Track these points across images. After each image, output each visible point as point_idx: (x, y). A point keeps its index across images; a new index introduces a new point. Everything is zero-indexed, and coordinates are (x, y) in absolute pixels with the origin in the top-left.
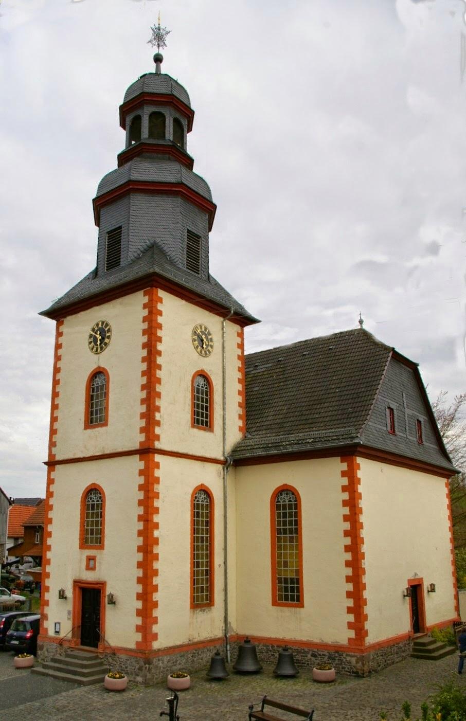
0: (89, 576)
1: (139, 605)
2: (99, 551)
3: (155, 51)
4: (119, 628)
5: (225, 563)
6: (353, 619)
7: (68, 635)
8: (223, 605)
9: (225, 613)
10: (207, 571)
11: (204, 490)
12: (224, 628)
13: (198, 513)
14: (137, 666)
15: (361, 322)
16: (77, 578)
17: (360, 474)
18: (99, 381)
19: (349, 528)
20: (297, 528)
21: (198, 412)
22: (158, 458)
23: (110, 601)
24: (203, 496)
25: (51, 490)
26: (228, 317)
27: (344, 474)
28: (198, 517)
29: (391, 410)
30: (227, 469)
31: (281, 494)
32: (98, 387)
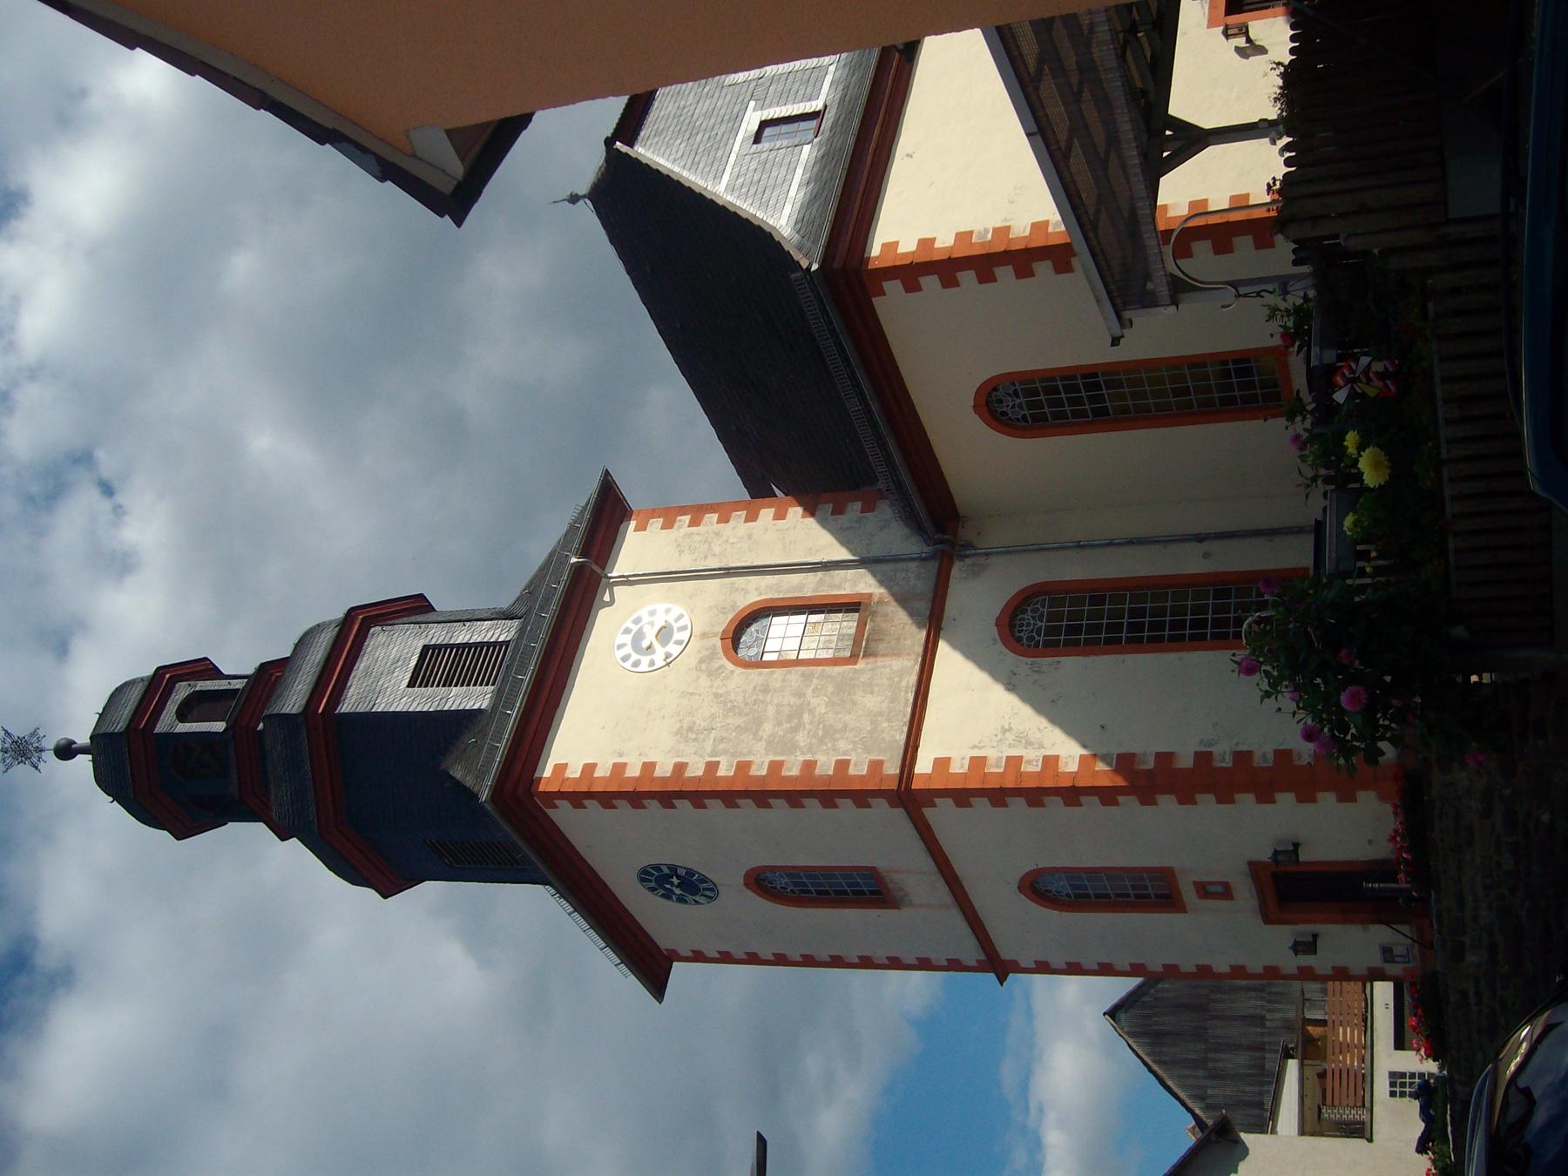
3: (50, 756)
5: (1199, 538)
11: (1013, 617)
15: (574, 199)
17: (908, 246)
19: (1049, 263)
22: (923, 766)
26: (598, 570)
29: (764, 124)
31: (1004, 414)
32: (1030, 405)
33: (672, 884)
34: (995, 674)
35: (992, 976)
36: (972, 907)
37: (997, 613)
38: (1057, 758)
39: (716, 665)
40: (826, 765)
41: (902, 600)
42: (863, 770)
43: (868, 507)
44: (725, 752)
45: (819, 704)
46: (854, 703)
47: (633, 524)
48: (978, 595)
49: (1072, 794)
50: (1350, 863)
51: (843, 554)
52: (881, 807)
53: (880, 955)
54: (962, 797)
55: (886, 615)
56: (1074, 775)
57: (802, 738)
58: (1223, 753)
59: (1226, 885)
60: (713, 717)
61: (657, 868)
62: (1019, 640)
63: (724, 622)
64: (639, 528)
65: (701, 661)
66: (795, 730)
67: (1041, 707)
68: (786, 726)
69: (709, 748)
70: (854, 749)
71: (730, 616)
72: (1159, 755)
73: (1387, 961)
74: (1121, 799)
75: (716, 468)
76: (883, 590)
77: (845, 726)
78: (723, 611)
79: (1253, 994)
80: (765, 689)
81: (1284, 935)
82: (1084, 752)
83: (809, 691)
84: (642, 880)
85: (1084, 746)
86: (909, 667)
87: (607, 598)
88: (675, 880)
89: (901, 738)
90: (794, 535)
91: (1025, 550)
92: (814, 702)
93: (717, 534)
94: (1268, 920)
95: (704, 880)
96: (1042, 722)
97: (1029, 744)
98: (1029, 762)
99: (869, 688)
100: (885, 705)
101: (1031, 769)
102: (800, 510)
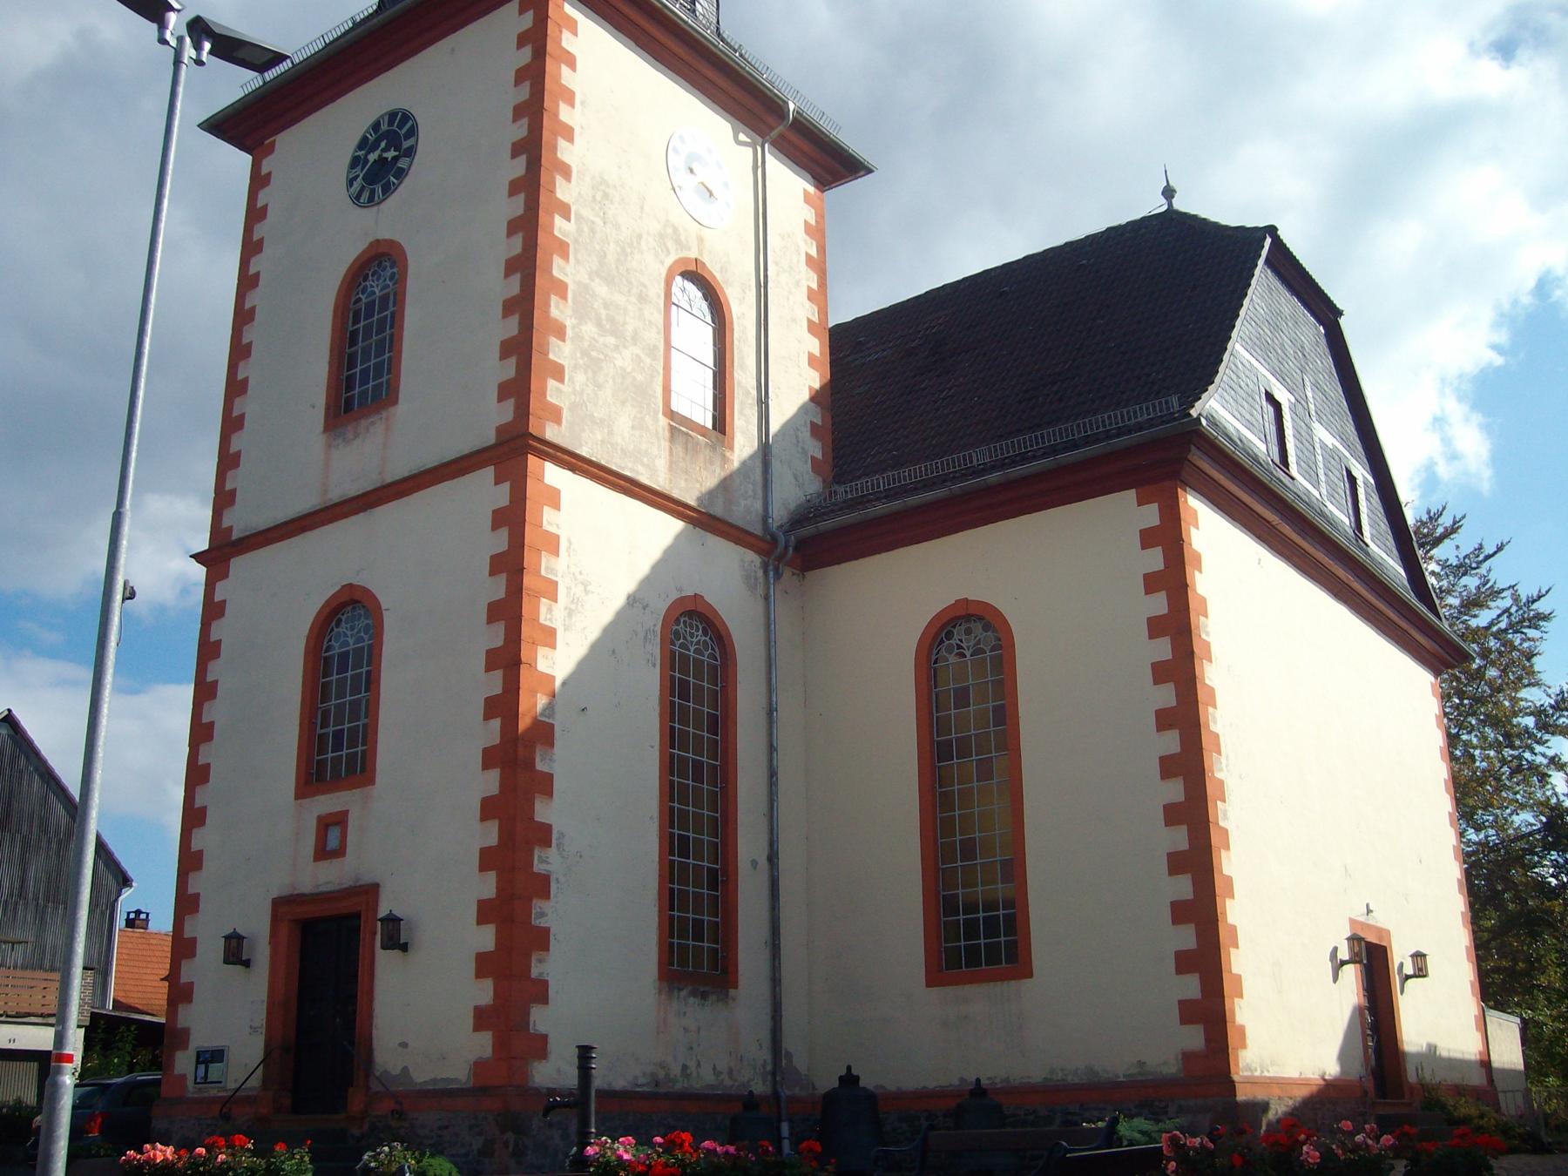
0: (330, 876)
1: (486, 938)
2: (357, 793)
4: (424, 1016)
5: (773, 858)
6: (1194, 939)
7: (249, 1084)
8: (764, 989)
9: (773, 1018)
10: (713, 873)
12: (769, 1068)
13: (684, 840)
14: (477, 1143)
15: (1169, 193)
16: (285, 892)
18: (347, 637)
20: (1015, 942)
21: (683, 815)
22: (554, 475)
23: (391, 938)
24: (700, 636)
25: (199, 802)
26: (774, 134)
27: (1148, 538)
28: (684, 853)
29: (1277, 406)
30: (776, 570)
31: (949, 635)
32: (344, 656)
33: (386, 150)
34: (646, 582)
35: (204, 545)
36: (323, 524)
37: (709, 599)
38: (553, 646)
39: (670, 244)
40: (560, 352)
41: (725, 485)
42: (551, 398)
43: (816, 465)
44: (580, 231)
45: (624, 359)
46: (623, 403)
47: (811, 189)
48: (727, 577)
49: (508, 660)
50: (370, 1017)
51: (774, 427)
52: (505, 413)
53: (247, 406)
54: (512, 519)
55: (711, 463)
56: (532, 666)
57: (589, 329)
58: (547, 861)
59: (340, 852)
60: (617, 227)
61: (413, 132)
62: (677, 621)
63: (715, 268)
64: (806, 193)
65: (675, 229)
66: (599, 324)
67: (610, 631)
68: (603, 313)
69: (585, 212)
70: (574, 392)
71: (718, 276)
72: (549, 778)
73: (199, 1054)
74: (496, 723)
75: (853, 305)
76: (736, 464)
77: (599, 387)
78: (723, 270)
79: (17, 885)
80: (642, 298)
81: (257, 926)
82: (558, 683)
83: (637, 351)
84: (392, 115)
85: (564, 684)
86: (656, 476)
87: (742, 137)
88: (390, 154)
89: (584, 452)
90: (796, 378)
91: (769, 643)
92: (627, 353)
93: (797, 283)
94: (277, 903)
95: (388, 190)
96: (594, 633)
97: (570, 613)
98: (550, 610)
99: (638, 425)
100: (620, 441)
101: (543, 610)
102: (817, 385)
